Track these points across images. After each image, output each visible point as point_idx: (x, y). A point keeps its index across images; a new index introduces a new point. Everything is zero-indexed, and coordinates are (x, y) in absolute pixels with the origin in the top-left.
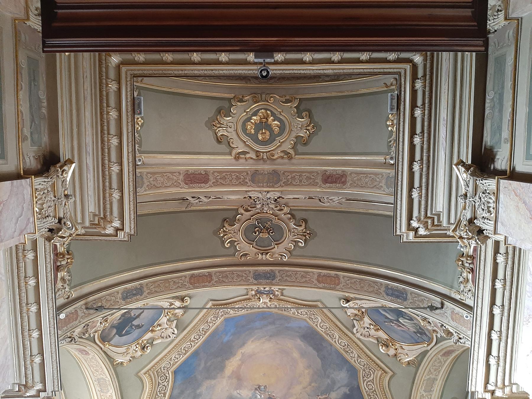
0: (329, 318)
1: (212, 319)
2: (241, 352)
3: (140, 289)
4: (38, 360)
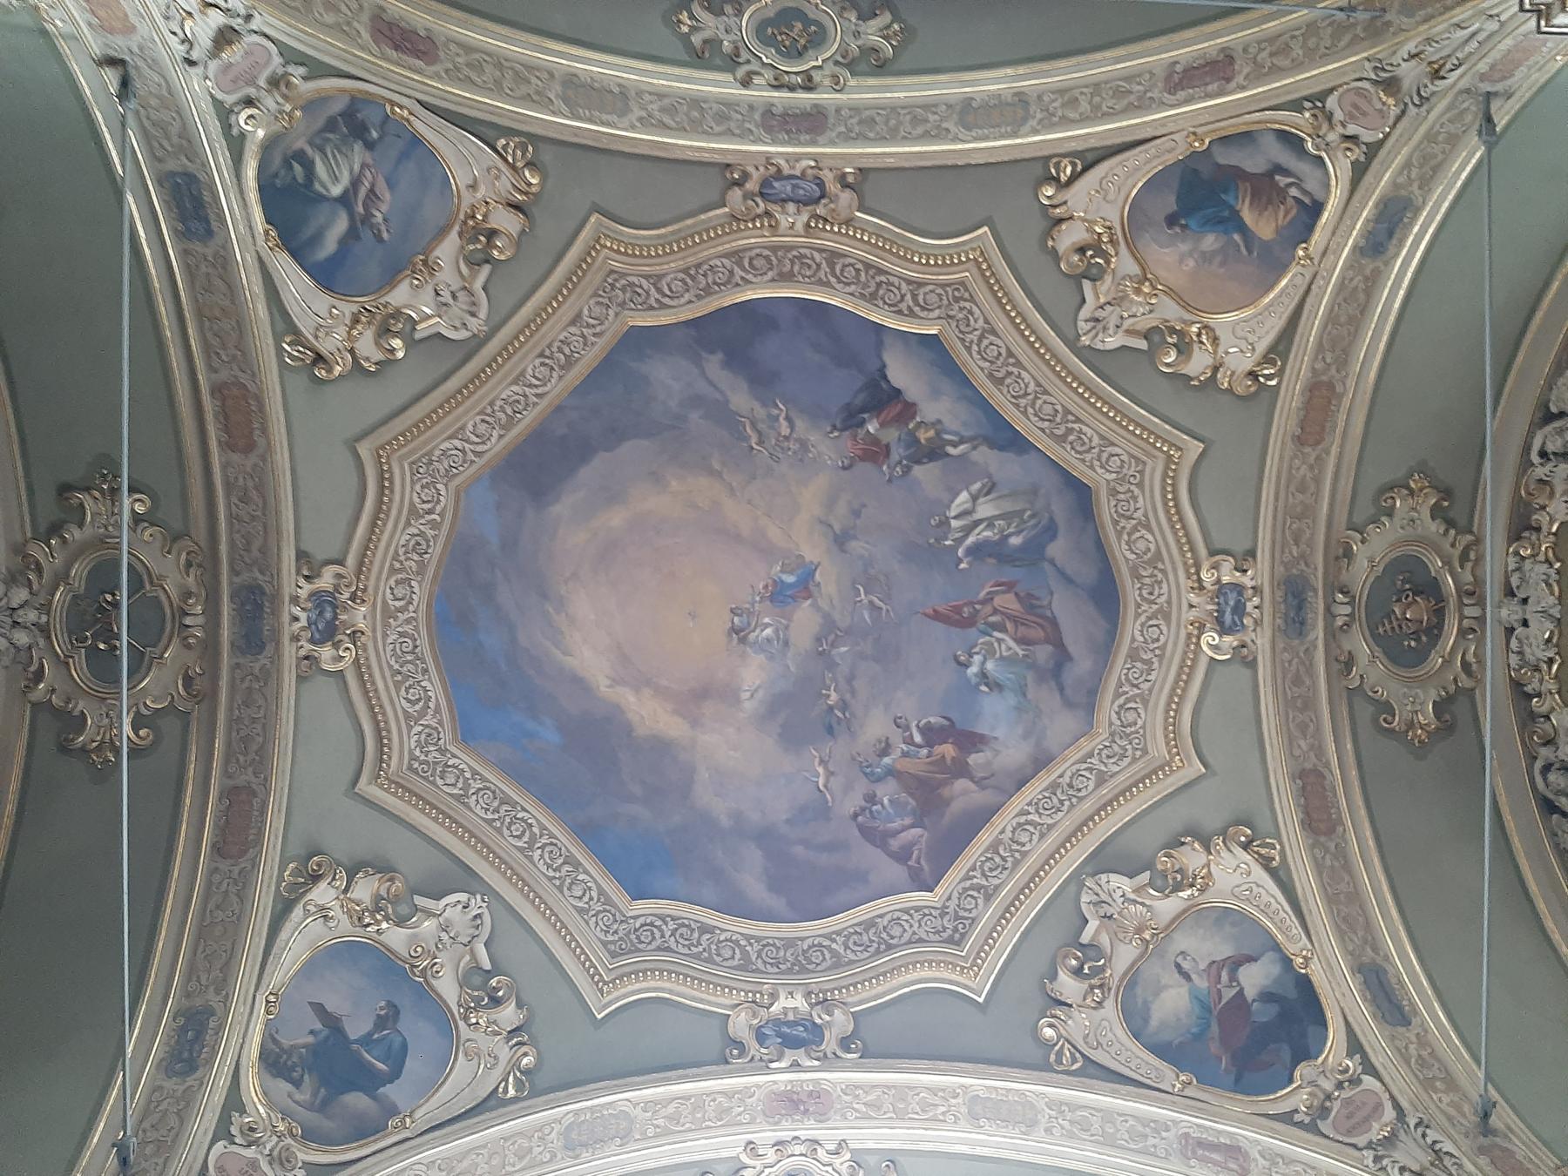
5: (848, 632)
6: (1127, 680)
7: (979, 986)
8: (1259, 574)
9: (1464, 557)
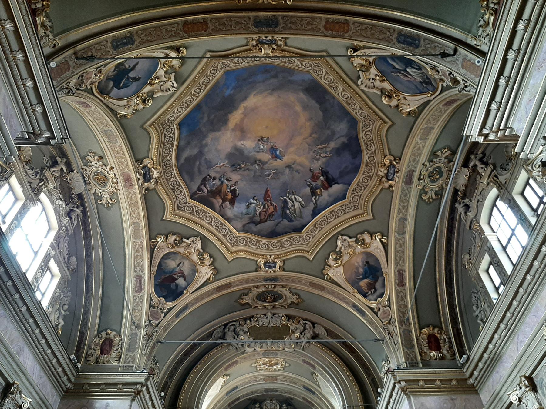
0: (334, 70)
1: (212, 72)
2: (244, 106)
3: (129, 37)
4: (39, 109)
5: (262, 168)
6: (251, 240)
7: (168, 216)
8: (279, 273)
9: (282, 306)
